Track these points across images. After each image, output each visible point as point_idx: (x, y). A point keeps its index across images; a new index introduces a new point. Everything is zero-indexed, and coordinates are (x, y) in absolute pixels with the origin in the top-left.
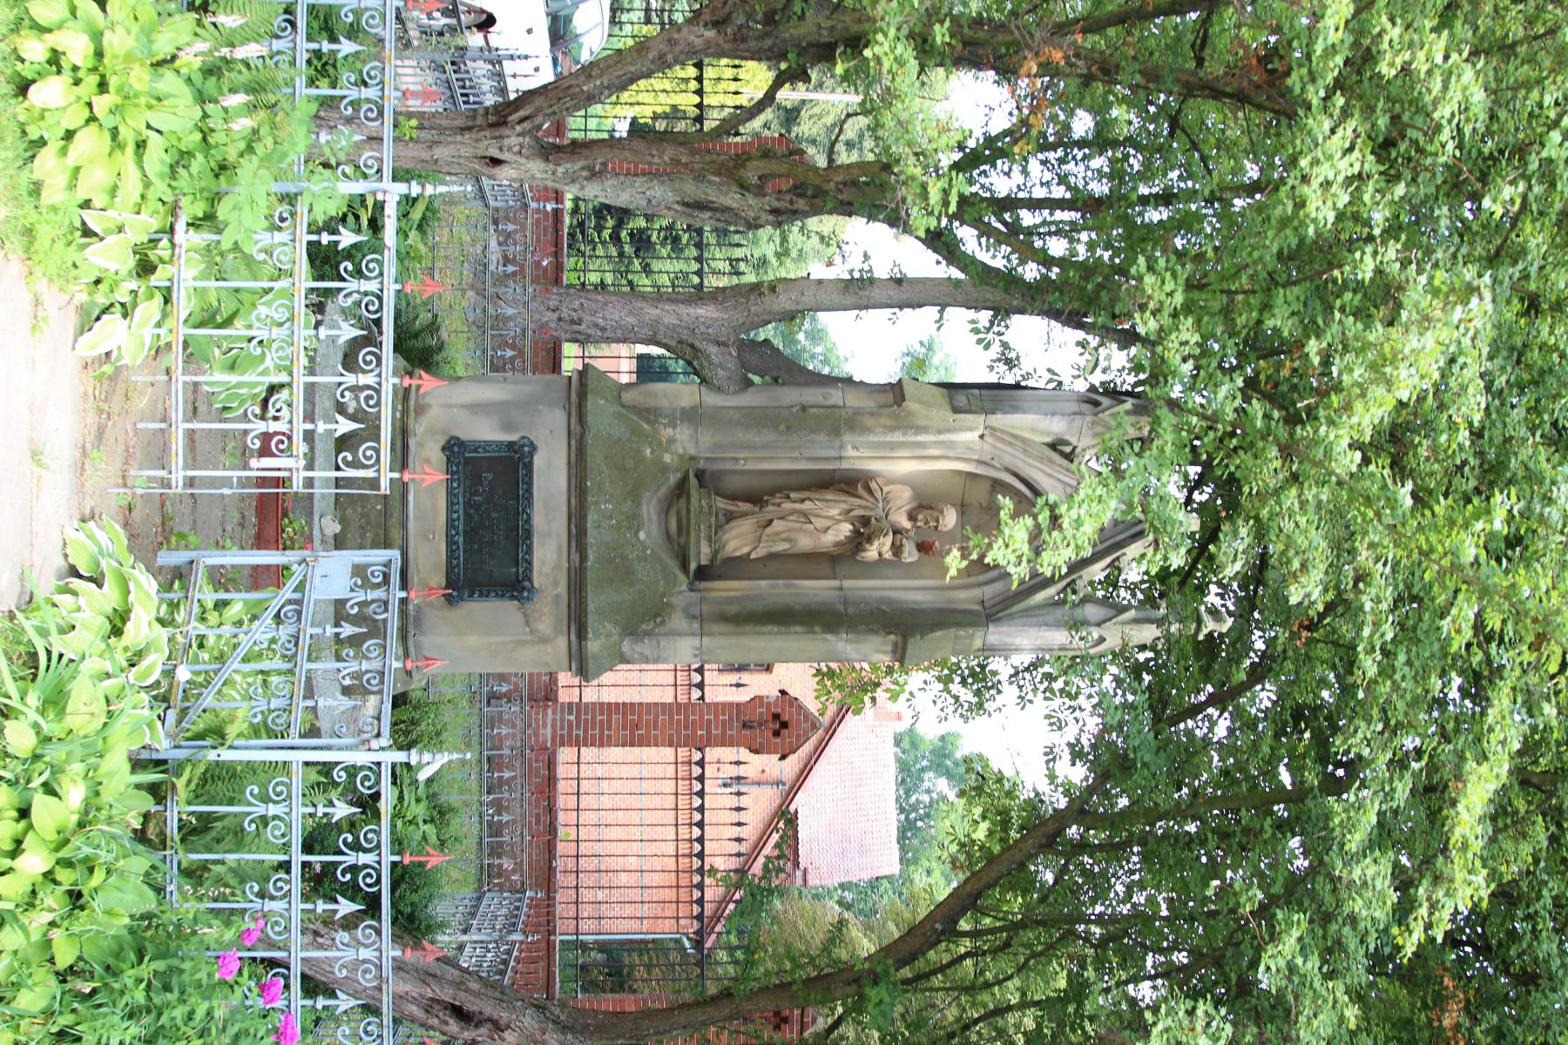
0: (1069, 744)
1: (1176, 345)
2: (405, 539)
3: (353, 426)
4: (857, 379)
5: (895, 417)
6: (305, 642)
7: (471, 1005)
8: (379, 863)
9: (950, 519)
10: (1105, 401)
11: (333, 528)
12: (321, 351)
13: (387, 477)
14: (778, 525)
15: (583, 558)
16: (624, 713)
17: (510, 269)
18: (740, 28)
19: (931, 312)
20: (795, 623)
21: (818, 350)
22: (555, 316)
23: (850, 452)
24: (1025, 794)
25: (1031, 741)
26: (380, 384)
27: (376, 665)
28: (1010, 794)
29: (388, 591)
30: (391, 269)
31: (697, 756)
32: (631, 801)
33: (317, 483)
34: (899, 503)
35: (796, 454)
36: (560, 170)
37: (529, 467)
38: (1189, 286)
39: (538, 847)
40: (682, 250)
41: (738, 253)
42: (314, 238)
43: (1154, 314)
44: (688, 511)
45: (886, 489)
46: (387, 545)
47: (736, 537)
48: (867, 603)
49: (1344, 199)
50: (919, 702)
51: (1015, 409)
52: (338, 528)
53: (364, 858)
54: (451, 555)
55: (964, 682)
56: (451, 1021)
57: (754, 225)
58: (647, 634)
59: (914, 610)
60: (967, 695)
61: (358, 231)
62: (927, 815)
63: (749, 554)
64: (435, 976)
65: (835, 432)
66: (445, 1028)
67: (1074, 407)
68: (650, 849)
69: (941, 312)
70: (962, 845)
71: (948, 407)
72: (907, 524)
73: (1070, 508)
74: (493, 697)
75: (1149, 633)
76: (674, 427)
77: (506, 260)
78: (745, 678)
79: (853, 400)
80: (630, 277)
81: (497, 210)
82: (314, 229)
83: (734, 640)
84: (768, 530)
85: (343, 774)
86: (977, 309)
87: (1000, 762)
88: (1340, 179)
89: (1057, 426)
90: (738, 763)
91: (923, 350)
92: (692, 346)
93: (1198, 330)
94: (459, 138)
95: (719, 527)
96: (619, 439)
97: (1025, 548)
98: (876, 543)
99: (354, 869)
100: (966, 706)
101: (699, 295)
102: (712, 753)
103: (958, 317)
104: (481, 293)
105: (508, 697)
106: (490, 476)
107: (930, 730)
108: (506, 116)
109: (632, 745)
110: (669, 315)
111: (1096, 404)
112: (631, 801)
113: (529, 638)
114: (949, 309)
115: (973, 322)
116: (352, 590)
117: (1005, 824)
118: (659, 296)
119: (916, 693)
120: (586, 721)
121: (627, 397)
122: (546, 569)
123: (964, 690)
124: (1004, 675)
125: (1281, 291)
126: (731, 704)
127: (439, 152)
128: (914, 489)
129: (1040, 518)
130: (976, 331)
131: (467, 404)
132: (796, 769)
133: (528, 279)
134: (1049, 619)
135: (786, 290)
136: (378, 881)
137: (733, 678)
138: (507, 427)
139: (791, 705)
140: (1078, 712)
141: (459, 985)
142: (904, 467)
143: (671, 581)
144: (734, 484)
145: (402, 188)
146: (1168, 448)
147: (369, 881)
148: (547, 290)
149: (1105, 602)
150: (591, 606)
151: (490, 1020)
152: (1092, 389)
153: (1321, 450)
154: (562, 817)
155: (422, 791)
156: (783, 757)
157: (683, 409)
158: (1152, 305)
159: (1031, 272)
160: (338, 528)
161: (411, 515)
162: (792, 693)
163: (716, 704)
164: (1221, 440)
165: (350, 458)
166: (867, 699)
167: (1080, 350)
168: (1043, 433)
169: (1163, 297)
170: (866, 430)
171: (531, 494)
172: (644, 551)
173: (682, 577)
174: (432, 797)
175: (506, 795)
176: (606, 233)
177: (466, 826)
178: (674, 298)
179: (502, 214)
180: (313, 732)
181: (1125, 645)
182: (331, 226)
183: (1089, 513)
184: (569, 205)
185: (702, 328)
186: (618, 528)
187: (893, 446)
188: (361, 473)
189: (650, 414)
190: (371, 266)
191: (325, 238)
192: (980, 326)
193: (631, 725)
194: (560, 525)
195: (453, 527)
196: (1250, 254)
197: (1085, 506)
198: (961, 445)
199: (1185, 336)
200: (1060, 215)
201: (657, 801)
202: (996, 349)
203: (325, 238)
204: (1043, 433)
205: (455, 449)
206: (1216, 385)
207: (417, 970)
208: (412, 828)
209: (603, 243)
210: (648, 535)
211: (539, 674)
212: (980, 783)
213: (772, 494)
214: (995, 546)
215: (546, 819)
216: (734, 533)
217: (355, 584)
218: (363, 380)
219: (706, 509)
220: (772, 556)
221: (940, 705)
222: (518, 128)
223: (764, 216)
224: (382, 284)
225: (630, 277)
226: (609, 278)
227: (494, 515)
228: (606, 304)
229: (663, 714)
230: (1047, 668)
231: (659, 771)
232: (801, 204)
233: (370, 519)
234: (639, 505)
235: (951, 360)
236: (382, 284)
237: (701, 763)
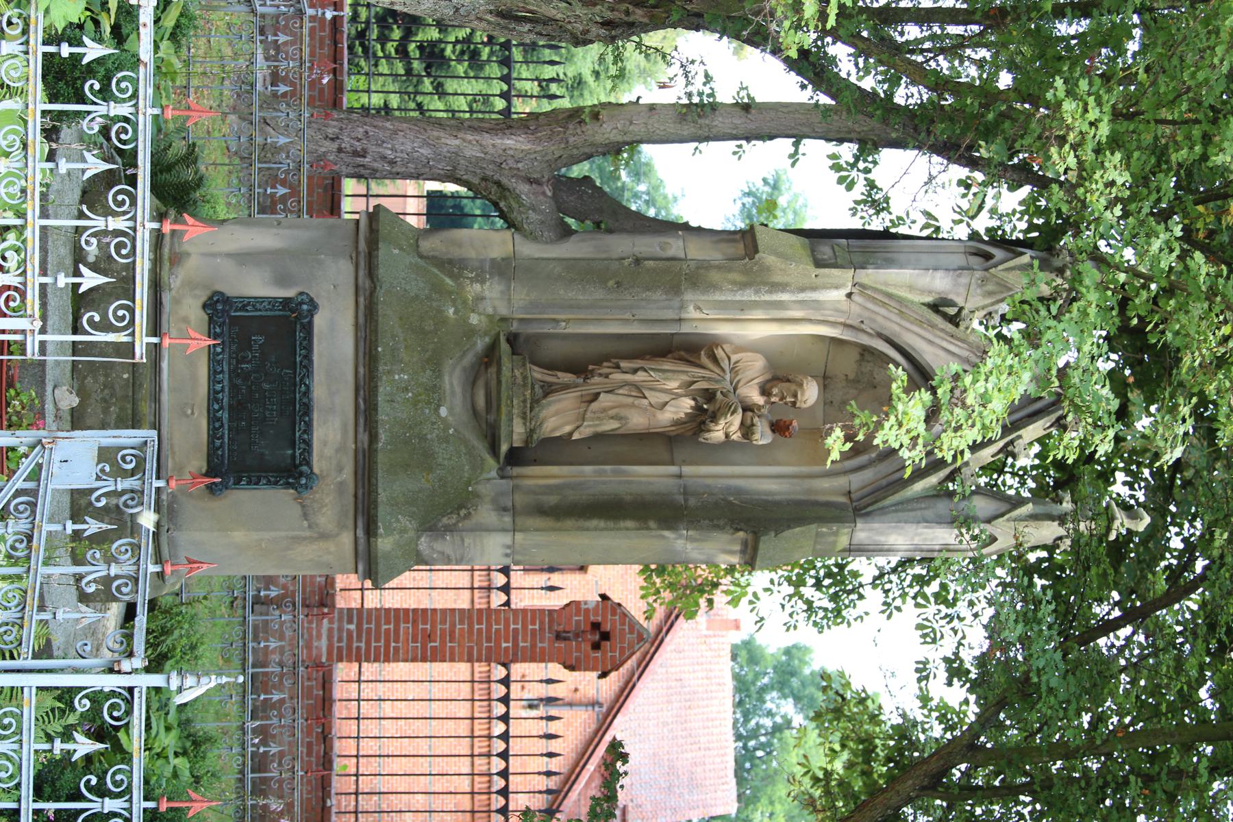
0: (946, 660)
1: (1101, 186)
2: (157, 414)
3: (100, 280)
4: (693, 224)
5: (746, 272)
6: (40, 543)
8: (130, 810)
9: (811, 393)
10: (998, 254)
11: (69, 400)
12: (55, 187)
13: (142, 341)
14: (605, 400)
15: (373, 438)
16: (415, 623)
17: (283, 89)
19: (784, 145)
20: (624, 517)
21: (642, 188)
22: (335, 146)
23: (692, 313)
24: (891, 718)
25: (900, 654)
27: (128, 569)
28: (874, 719)
29: (142, 479)
30: (146, 91)
31: (499, 672)
33: (50, 348)
34: (750, 374)
35: (626, 316)
37: (308, 329)
38: (1116, 115)
39: (309, 782)
40: (481, 68)
41: (549, 72)
42: (51, 49)
43: (1074, 147)
44: (499, 382)
45: (734, 358)
46: (135, 422)
47: (556, 414)
48: (711, 494)
50: (761, 608)
51: (889, 263)
52: (75, 401)
53: (110, 805)
54: (213, 434)
55: (818, 585)
57: (581, 41)
58: (450, 529)
59: (767, 502)
60: (821, 600)
61: (100, 41)
63: (571, 434)
65: (675, 289)
67: (960, 260)
68: (439, 784)
69: (796, 145)
70: (816, 780)
71: (809, 260)
72: (759, 399)
73: (975, 381)
75: (1049, 531)
76: (483, 282)
77: (275, 78)
78: (556, 579)
79: (696, 251)
80: (419, 98)
81: (263, 16)
82: (52, 38)
83: (553, 537)
84: (594, 406)
85: (86, 702)
86: (841, 141)
87: (862, 679)
89: (940, 283)
90: (550, 681)
91: (767, 189)
92: (498, 184)
93: (1128, 167)
95: (535, 402)
96: (417, 296)
97: (922, 428)
98: (722, 422)
100: (821, 614)
101: (507, 122)
102: (518, 669)
103: (816, 150)
104: (247, 118)
105: (278, 602)
106: (260, 339)
107: (773, 641)
109: (424, 660)
110: (470, 147)
111: (988, 257)
113: (307, 533)
114: (805, 141)
115: (833, 157)
116: (98, 478)
117: (868, 753)
118: (455, 123)
119: (761, 594)
120: (369, 631)
121: (426, 245)
122: (329, 451)
123: (818, 595)
124: (866, 578)
126: (542, 611)
129: (940, 391)
130: (837, 168)
131: (233, 251)
133: (305, 100)
134: (929, 513)
137: (541, 579)
138: (282, 279)
139: (614, 613)
140: (956, 623)
142: (759, 331)
143: (477, 466)
146: (1092, 310)
148: (327, 116)
149: (992, 492)
150: (383, 496)
152: (974, 236)
154: (339, 746)
155: (172, 717)
156: (604, 675)
157: (493, 260)
158: (1071, 137)
159: (908, 95)
160: (75, 401)
162: (615, 597)
163: (524, 611)
164: (1155, 301)
165: (97, 318)
166: (703, 602)
167: (962, 190)
168: (923, 291)
169: (1085, 128)
170: (714, 287)
171: (311, 361)
172: (447, 427)
173: (491, 461)
174: (184, 724)
175: (275, 721)
176: (391, 47)
177: (224, 759)
178: (477, 127)
179: (268, 21)
180: (45, 651)
181: (1019, 545)
182: (73, 34)
183: (999, 385)
184: (347, 12)
185: (511, 162)
186: (415, 403)
187: (743, 306)
188: (111, 337)
189: (453, 266)
190: (123, 85)
191: (66, 50)
192: (842, 162)
193: (424, 636)
194: (345, 399)
195: (217, 400)
196: (1193, 76)
197: (992, 379)
198: (823, 306)
199: (1112, 175)
202: (860, 189)
203: (66, 50)
204: (923, 291)
205: (220, 309)
206: (1148, 236)
208: (160, 762)
209: (387, 57)
210: (451, 410)
211: (314, 576)
212: (839, 707)
213: (599, 362)
214: (887, 425)
216: (553, 409)
217: (102, 471)
218: (115, 224)
219: (519, 380)
220: (598, 437)
221: (788, 610)
223: (595, 30)
224: (139, 109)
225: (419, 98)
226: (394, 101)
227: (266, 386)
228: (395, 132)
229: (462, 622)
230: (918, 570)
231: (452, 691)
232: (639, 15)
233: (116, 391)
235: (800, 202)
236: (139, 109)
237: (506, 682)
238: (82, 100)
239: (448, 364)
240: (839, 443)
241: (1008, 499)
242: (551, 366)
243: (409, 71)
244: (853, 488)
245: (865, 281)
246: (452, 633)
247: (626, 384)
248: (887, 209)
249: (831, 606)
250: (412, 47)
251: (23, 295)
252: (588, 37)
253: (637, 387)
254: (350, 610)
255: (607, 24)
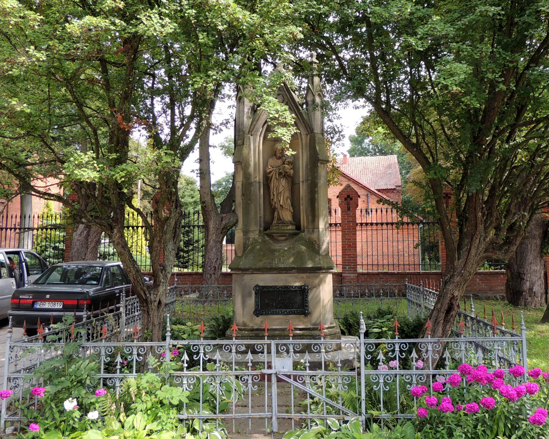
7: (446, 307)
8: (398, 343)
15: (294, 268)
16: (345, 250)
18: (113, 221)
19: (211, 150)
21: (224, 183)
22: (213, 275)
26: (235, 344)
30: (196, 342)
32: (375, 244)
36: (162, 280)
37: (263, 287)
44: (278, 233)
49: (167, 20)
50: (339, 150)
53: (397, 349)
56: (451, 314)
62: (377, 146)
64: (436, 319)
65: (251, 184)
66: (454, 316)
68: (390, 239)
69: (211, 146)
74: (341, 295)
76: (249, 238)
88: (160, 21)
92: (223, 229)
94: (151, 316)
95: (283, 223)
99: (401, 351)
102: (359, 221)
104: (205, 302)
108: (144, 300)
110: (213, 237)
112: (375, 244)
118: (206, 237)
125: (200, 40)
127: (156, 322)
128: (270, 158)
130: (216, 133)
131: (242, 309)
132: (363, 190)
133: (200, 286)
135: (204, 198)
136: (405, 343)
137: (333, 212)
141: (439, 311)
144: (268, 218)
145: (168, 339)
147: (405, 347)
151: (450, 300)
153: (252, 28)
161: (280, 327)
162: (338, 194)
172: (291, 248)
173: (300, 235)
176: (185, 255)
193: (349, 246)
194: (283, 276)
200: (177, 111)
201: (374, 236)
202: (223, 128)
205: (257, 313)
207: (434, 326)
209: (189, 256)
213: (271, 205)
215: (381, 276)
219: (277, 227)
222: (148, 295)
232: (174, 198)
234: (276, 250)
238: (199, 360)
239: (273, 247)
240: (290, 152)
241: (307, 92)
242: (273, 219)
243: (192, 250)
244: (305, 133)
245: (248, 131)
246: (348, 239)
247: (277, 197)
248: (228, 120)
249: (338, 134)
250: (185, 249)
251: (254, 375)
252: (180, 212)
253: (278, 194)
254: (343, 268)
255: (176, 207)
